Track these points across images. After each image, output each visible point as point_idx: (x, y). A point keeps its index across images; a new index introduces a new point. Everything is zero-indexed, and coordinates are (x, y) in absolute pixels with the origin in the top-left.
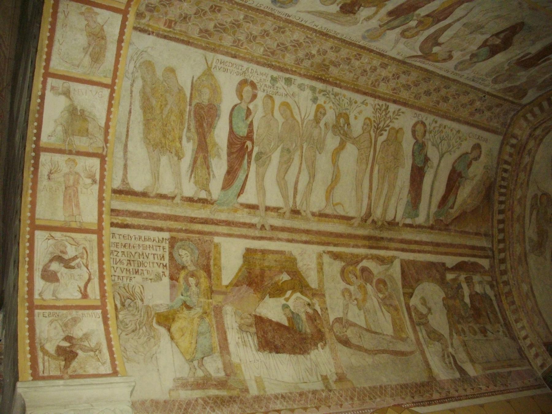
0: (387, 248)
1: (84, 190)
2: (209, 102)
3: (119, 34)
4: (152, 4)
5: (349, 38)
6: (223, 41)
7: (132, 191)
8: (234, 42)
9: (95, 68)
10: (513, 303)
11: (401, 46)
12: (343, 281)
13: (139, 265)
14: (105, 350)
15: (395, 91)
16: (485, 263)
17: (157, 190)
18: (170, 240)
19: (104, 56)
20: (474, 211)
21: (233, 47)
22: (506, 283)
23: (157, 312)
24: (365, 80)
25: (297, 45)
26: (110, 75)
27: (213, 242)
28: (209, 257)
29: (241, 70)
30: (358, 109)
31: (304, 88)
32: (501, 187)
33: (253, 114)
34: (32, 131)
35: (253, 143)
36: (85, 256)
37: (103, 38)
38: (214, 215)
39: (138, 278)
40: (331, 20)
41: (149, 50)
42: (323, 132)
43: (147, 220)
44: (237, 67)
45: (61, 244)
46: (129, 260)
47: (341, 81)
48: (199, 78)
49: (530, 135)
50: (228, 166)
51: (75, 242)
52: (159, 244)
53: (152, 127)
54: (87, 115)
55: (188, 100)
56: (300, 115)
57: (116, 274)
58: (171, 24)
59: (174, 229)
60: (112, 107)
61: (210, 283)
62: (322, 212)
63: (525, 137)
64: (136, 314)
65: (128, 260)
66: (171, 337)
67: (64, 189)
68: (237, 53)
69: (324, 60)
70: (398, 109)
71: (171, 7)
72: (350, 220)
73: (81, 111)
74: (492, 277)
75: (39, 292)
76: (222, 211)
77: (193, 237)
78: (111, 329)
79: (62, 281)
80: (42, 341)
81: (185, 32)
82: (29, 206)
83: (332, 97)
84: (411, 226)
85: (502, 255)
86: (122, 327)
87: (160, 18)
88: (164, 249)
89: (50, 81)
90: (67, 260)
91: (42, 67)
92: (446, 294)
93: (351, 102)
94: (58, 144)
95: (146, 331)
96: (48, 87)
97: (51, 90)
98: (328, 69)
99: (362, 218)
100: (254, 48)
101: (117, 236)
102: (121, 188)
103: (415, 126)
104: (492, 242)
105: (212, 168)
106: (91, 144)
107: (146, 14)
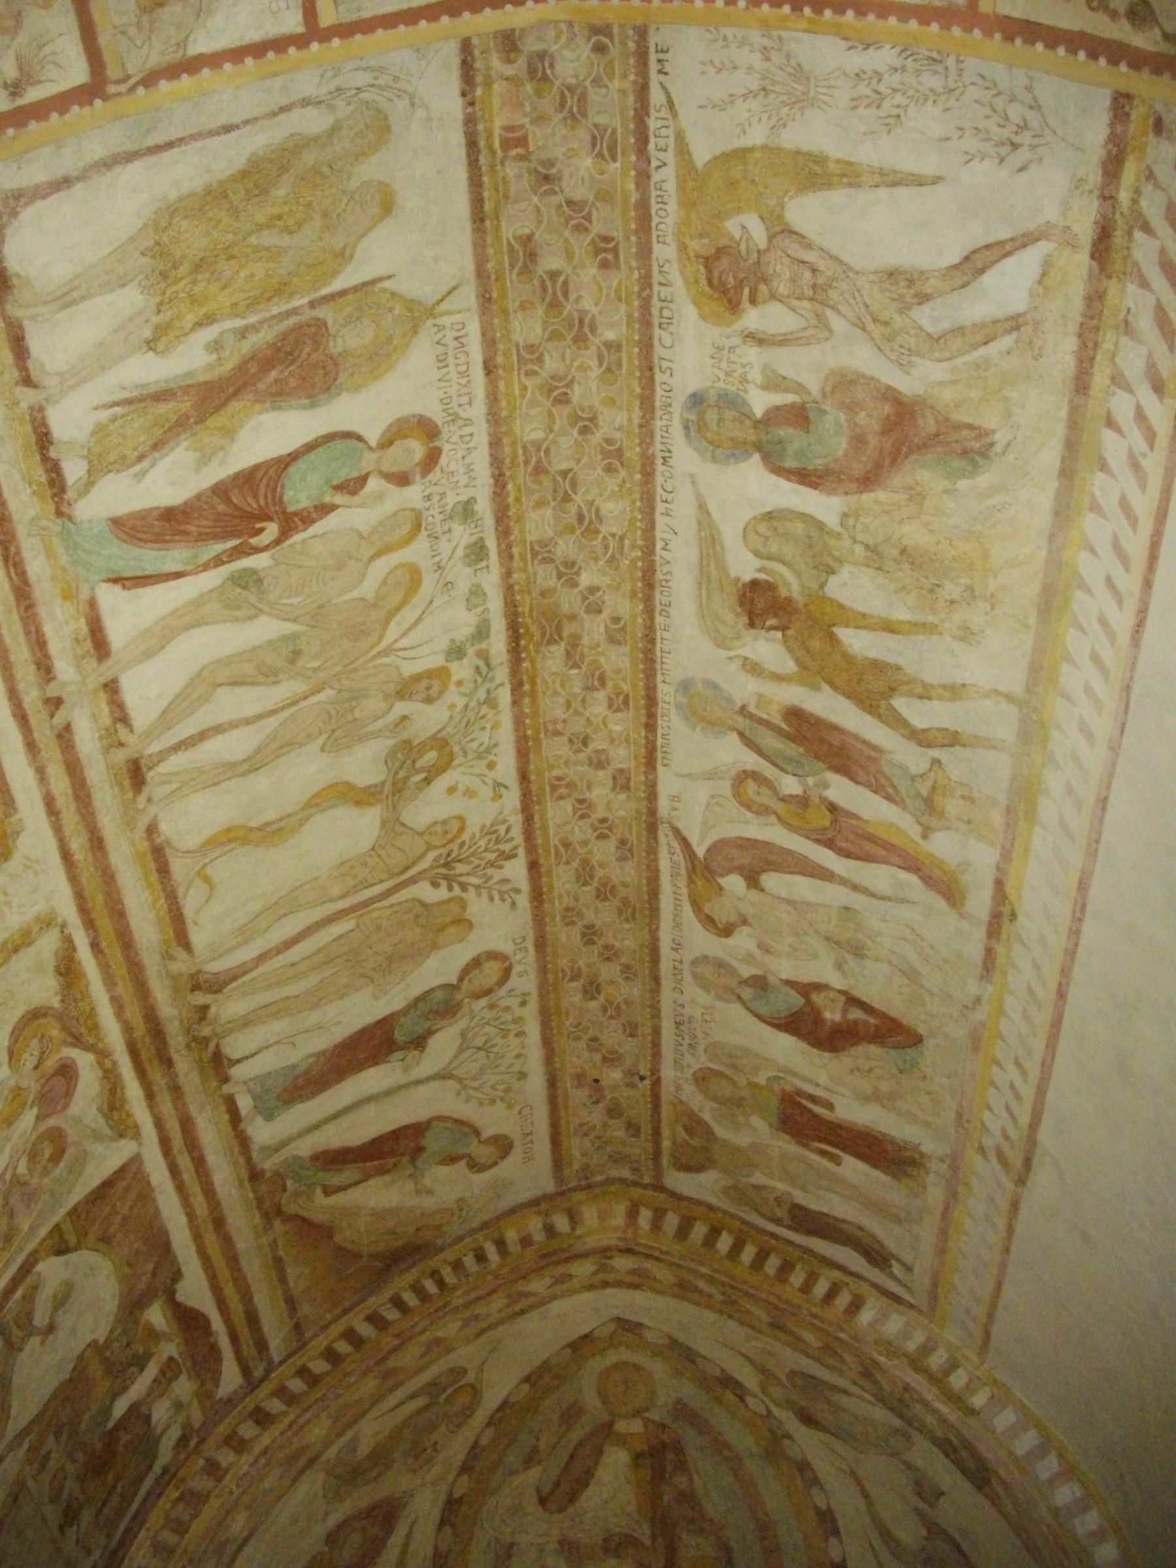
0: (150, 1096)
2: (340, 354)
4: (552, 66)
5: (665, 648)
8: (531, 348)
10: (180, 1528)
11: (702, 792)
12: (12, 1034)
15: (562, 850)
16: (231, 1377)
17: (32, 318)
20: (346, 1255)
21: (514, 351)
22: (214, 1469)
24: (560, 757)
25: (586, 522)
26: (347, 15)
29: (460, 405)
30: (475, 783)
31: (476, 606)
32: (435, 1274)
33: (357, 499)
35: (277, 542)
38: (29, 535)
40: (704, 577)
41: (420, 113)
42: (379, 724)
44: (464, 390)
47: (533, 694)
48: (393, 294)
49: (605, 1252)
50: (185, 503)
53: (211, 214)
55: (325, 291)
56: (404, 634)
58: (516, 147)
60: (255, 57)
62: (168, 851)
63: (592, 1242)
68: (501, 372)
69: (572, 617)
70: (515, 885)
72: (179, 944)
74: (204, 1424)
76: (50, 554)
83: (482, 695)
84: (235, 1117)
85: (275, 1406)
87: (522, 105)
92: (109, 1341)
93: (486, 753)
98: (551, 641)
99: (199, 972)
100: (533, 412)
103: (493, 956)
104: (288, 1357)
105: (162, 457)
107: (520, 61)
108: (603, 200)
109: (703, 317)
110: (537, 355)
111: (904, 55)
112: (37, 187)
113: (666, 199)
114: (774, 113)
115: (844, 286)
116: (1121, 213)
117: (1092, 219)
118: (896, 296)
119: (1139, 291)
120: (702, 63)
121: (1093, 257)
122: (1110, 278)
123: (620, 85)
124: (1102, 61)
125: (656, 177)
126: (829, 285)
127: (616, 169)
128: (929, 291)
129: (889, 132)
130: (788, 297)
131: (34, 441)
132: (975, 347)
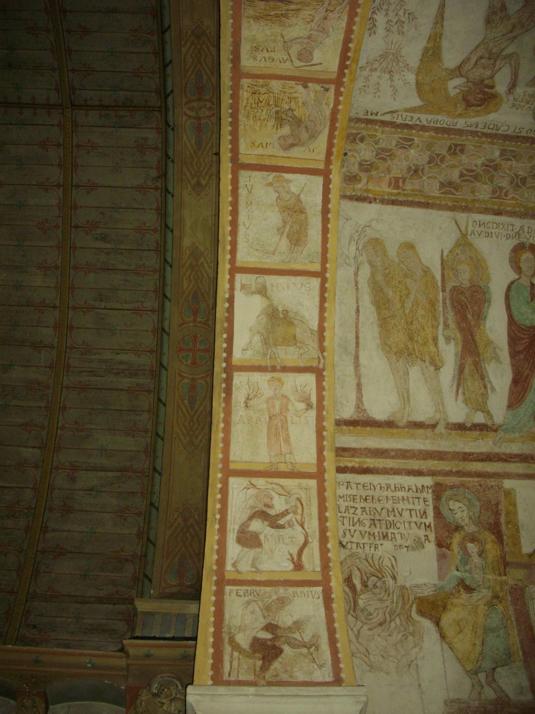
1: (296, 419)
2: (470, 283)
3: (322, 202)
4: (366, 161)
6: (476, 194)
7: (371, 421)
8: (494, 192)
9: (296, 252)
13: (389, 526)
14: (325, 646)
18: (434, 488)
19: (306, 235)
21: (494, 200)
23: (418, 595)
27: (502, 487)
28: (498, 511)
29: (512, 230)
34: (220, 345)
36: (300, 511)
37: (301, 212)
38: (500, 447)
39: (388, 545)
41: (374, 224)
43: (397, 461)
44: (506, 227)
45: (265, 495)
46: (374, 520)
48: (451, 252)
50: (513, 373)
51: (286, 491)
52: (418, 495)
53: (391, 327)
54: (292, 316)
55: (440, 284)
57: (354, 540)
59: (439, 472)
61: (502, 550)
64: (385, 597)
65: (371, 520)
66: (441, 634)
67: (268, 419)
68: (502, 208)
71: (394, 159)
73: (284, 312)
75: (233, 561)
76: (512, 441)
77: (470, 482)
78: (335, 615)
79: (266, 546)
80: (233, 631)
82: (221, 445)
86: (363, 619)
87: (381, 177)
88: (425, 501)
89: (239, 278)
90: (273, 517)
91: (227, 262)
94: (258, 360)
95: (401, 625)
96: (238, 286)
100: (526, 196)
101: (354, 486)
102: (355, 417)
105: (488, 377)
106: (302, 354)
107: (361, 175)
110: (498, 190)
112: (357, 398)
113: (435, 120)
114: (401, 69)
120: (375, 97)
125: (425, 123)
128: (500, 4)
129: (416, 18)
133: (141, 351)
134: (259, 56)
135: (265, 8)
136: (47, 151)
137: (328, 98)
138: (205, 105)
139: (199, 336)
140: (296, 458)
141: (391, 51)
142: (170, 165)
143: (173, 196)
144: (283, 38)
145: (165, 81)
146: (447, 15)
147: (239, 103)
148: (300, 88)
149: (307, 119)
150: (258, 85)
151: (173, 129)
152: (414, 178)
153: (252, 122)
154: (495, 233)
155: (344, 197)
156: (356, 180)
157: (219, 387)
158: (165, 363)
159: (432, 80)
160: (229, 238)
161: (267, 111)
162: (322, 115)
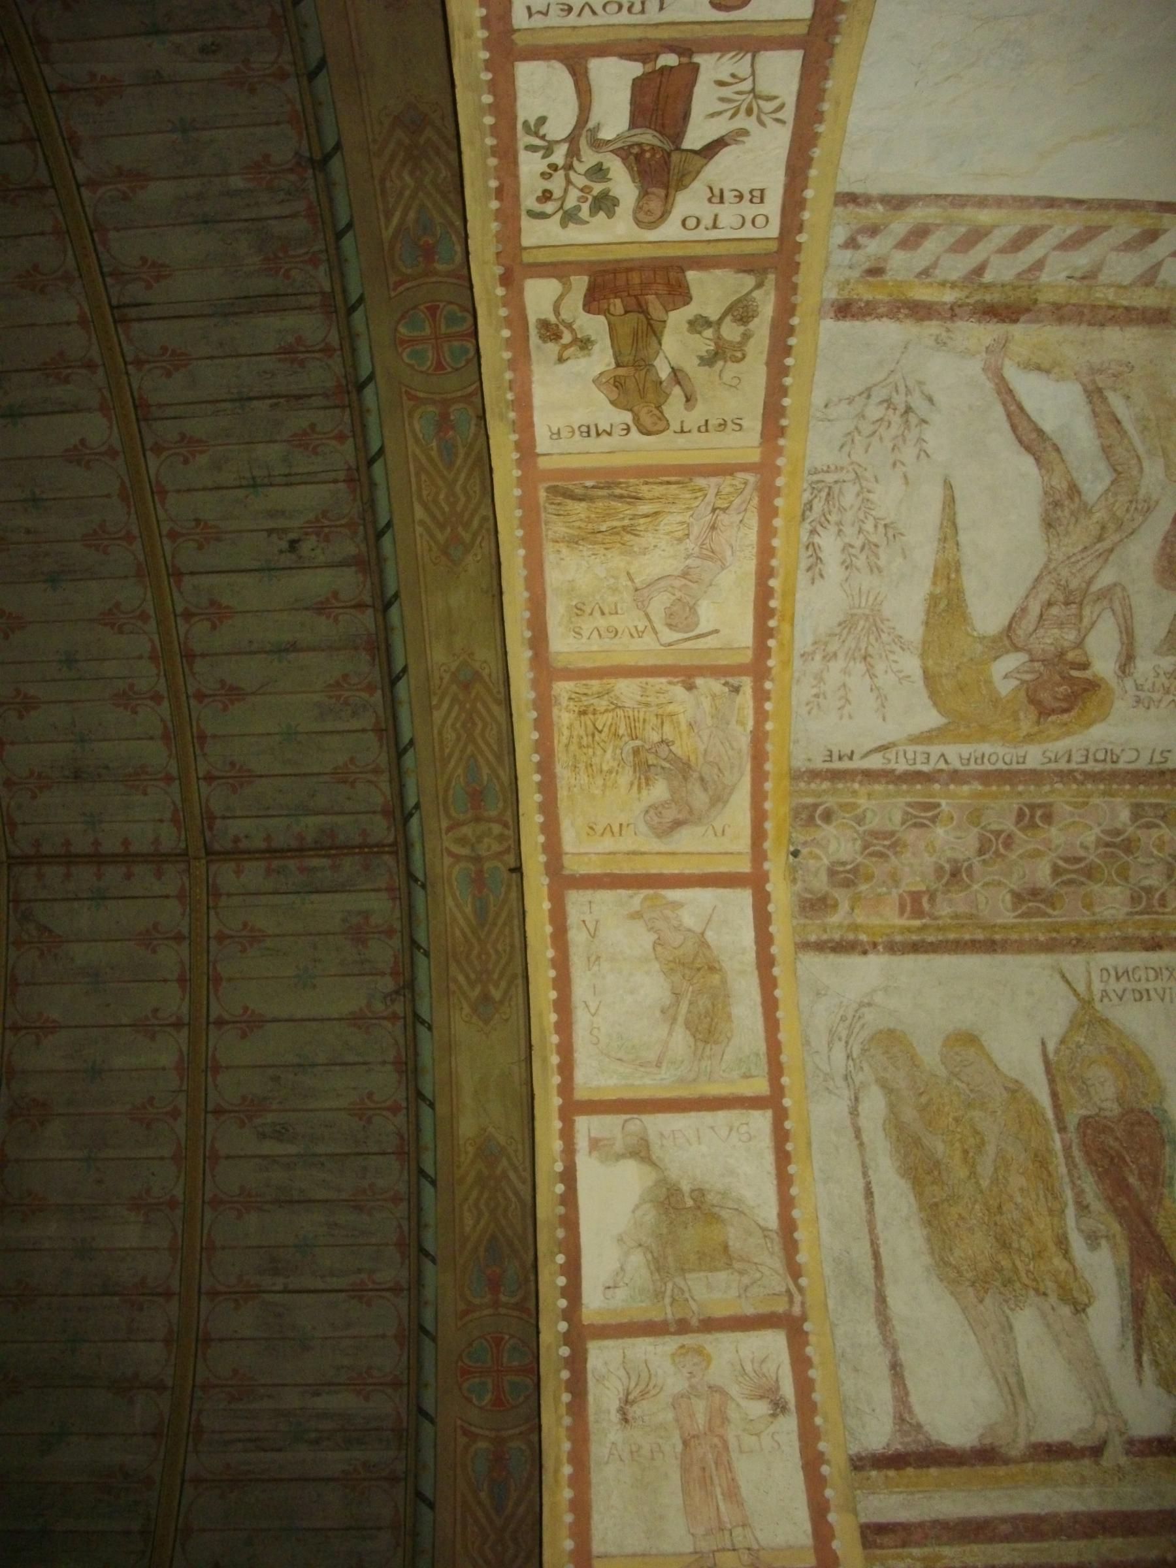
1: (749, 1441)
4: (844, 864)
6: (1097, 910)
7: (938, 1451)
8: (1135, 899)
9: (710, 1058)
17: (1029, 1431)
21: (1137, 917)
26: (761, 1068)
34: (551, 1280)
37: (712, 969)
41: (879, 998)
43: (1019, 1545)
48: (1062, 1042)
53: (952, 1224)
54: (715, 1202)
55: (1050, 1114)
58: (920, 904)
68: (1159, 933)
71: (902, 853)
81: (971, 916)
87: (879, 895)
89: (584, 1125)
91: (554, 1092)
94: (644, 1310)
96: (582, 1143)
97: (590, 1152)
106: (746, 1288)
107: (837, 895)
108: (979, 817)
109: (1103, 718)
111: (826, 524)
112: (895, 1398)
113: (979, 755)
114: (888, 647)
115: (1065, 573)
116: (967, 297)
117: (976, 325)
118: (1073, 520)
119: (1047, 269)
121: (1016, 321)
122: (1036, 301)
123: (864, 798)
124: (792, 341)
125: (956, 764)
126: (1064, 588)
127: (948, 804)
128: (1065, 485)
129: (902, 535)
130: (1079, 630)
131: (1166, 1458)
132: (1123, 433)
133: (371, 1384)
134: (587, 626)
135: (588, 517)
136: (154, 951)
137: (741, 708)
138: (490, 829)
139: (507, 1337)
140: (758, 1534)
141: (860, 611)
142: (421, 959)
143: (430, 1028)
144: (632, 580)
145: (402, 786)
146: (961, 520)
147: (553, 738)
148: (679, 691)
149: (701, 760)
150: (590, 692)
151: (424, 886)
152: (952, 889)
153: (584, 778)
154: (1155, 990)
155: (805, 946)
156: (826, 906)
157: (553, 1377)
158: (428, 1405)
159: (955, 664)
160: (555, 1039)
161: (614, 751)
162: (733, 749)
